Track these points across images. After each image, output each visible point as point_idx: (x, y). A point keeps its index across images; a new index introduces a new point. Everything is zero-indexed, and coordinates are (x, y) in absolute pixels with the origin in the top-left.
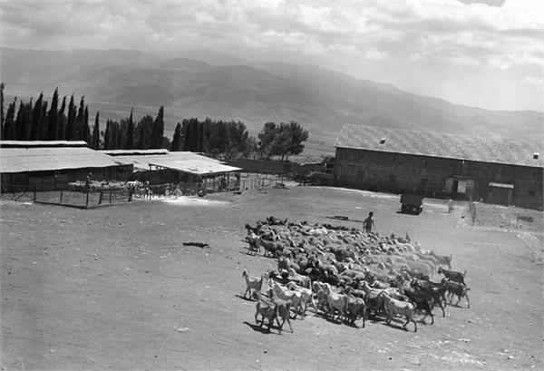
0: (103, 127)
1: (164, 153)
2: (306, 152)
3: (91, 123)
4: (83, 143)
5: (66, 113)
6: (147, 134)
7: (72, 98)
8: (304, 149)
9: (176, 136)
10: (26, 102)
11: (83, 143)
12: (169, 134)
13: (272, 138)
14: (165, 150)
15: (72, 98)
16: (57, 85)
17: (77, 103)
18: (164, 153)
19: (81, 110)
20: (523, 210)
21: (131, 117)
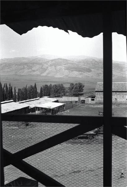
0: (17, 91)
1: (39, 99)
2: (84, 91)
3: (13, 91)
4: (12, 100)
5: (5, 88)
6: (30, 93)
7: (6, 84)
8: (84, 90)
9: (41, 91)
10: (21, 88)
11: (12, 100)
12: (39, 91)
13: (73, 88)
14: (38, 98)
15: (6, 84)
16: (27, 83)
17: (8, 86)
18: (39, 99)
19: (10, 88)
20: (26, 175)
21: (26, 87)
